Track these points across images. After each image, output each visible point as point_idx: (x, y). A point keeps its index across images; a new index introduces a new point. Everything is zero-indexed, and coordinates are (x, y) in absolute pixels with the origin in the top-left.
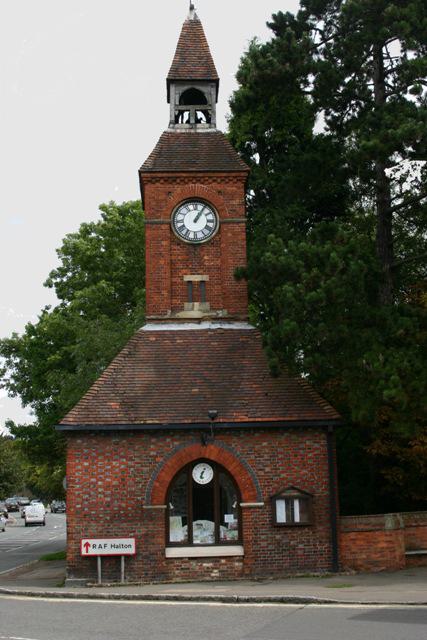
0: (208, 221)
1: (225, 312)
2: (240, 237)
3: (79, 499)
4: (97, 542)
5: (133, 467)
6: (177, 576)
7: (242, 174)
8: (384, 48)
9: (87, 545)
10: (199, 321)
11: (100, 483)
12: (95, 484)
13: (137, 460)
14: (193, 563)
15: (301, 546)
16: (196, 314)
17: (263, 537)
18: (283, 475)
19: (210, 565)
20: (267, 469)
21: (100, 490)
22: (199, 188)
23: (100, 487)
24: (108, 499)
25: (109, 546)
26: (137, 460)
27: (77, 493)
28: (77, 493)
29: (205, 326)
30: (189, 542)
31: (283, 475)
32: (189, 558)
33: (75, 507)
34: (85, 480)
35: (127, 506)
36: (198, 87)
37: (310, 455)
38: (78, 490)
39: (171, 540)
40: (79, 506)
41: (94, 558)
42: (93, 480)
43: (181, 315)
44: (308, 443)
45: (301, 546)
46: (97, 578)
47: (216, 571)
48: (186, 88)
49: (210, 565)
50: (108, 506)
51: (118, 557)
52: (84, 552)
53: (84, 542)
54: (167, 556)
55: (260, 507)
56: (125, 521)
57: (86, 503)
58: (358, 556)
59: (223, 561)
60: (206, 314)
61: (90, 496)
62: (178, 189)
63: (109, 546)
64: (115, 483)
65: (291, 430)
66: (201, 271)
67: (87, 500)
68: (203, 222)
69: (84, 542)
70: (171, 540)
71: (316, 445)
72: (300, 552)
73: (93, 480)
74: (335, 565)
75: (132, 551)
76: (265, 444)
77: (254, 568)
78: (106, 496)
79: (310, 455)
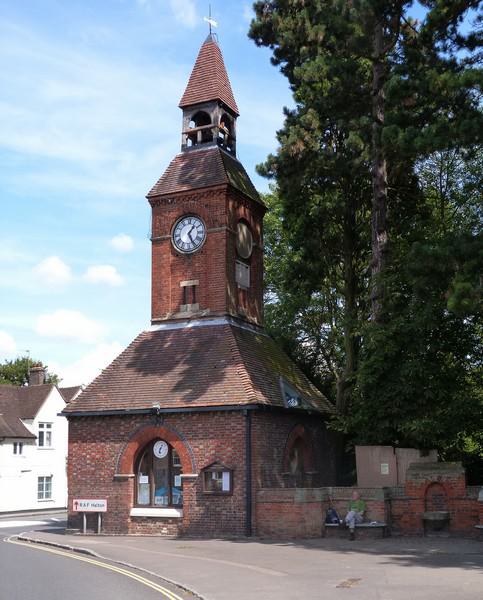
0: (198, 232)
1: (208, 310)
4: (83, 501)
8: (401, 19)
9: (76, 503)
10: (189, 320)
16: (187, 315)
20: (201, 447)
30: (150, 505)
36: (203, 110)
37: (234, 435)
41: (81, 513)
44: (233, 424)
45: (224, 512)
46: (83, 528)
48: (195, 112)
51: (97, 514)
52: (74, 509)
53: (74, 501)
55: (195, 478)
58: (271, 524)
64: (97, 456)
68: (185, 238)
69: (74, 501)
71: (239, 427)
74: (249, 529)
75: (104, 509)
76: (200, 425)
77: (186, 532)
79: (234, 435)
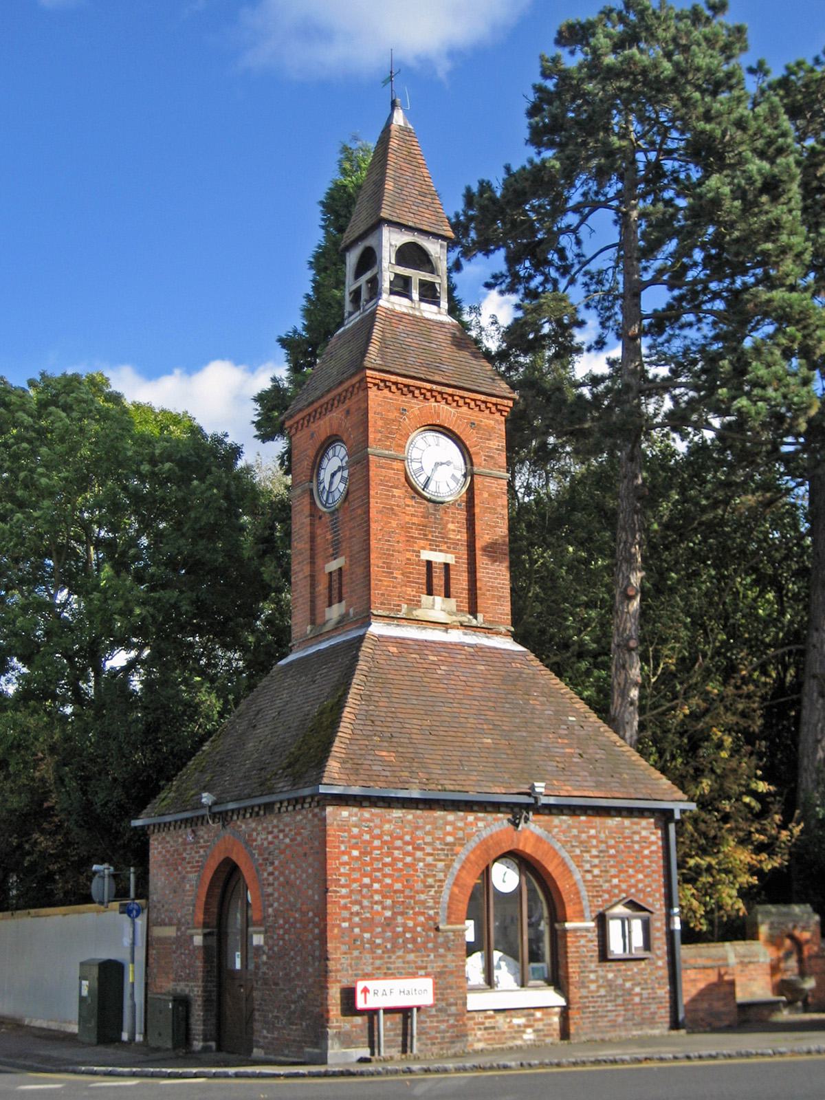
2: (500, 502)
3: (346, 914)
5: (424, 860)
6: (479, 1040)
7: (505, 402)
10: (446, 626)
11: (376, 886)
12: (369, 886)
13: (429, 849)
14: (500, 1018)
15: (637, 990)
17: (592, 976)
18: (615, 881)
19: (522, 1021)
20: (596, 871)
21: (377, 897)
22: (447, 413)
23: (376, 892)
24: (388, 914)
25: (396, 992)
26: (429, 849)
27: (343, 902)
28: (343, 902)
29: (455, 636)
31: (615, 881)
32: (496, 1011)
33: (339, 926)
34: (355, 881)
35: (416, 925)
38: (343, 897)
39: (366, 1018)
40: (345, 925)
42: (367, 880)
43: (419, 613)
45: (637, 990)
47: (529, 1030)
49: (522, 1021)
50: (388, 925)
54: (469, 1007)
56: (412, 951)
57: (357, 919)
59: (538, 1014)
60: (454, 618)
61: (362, 908)
62: (416, 406)
63: (396, 992)
65: (624, 813)
66: (444, 547)
67: (358, 914)
70: (366, 1018)
72: (637, 999)
73: (367, 880)
75: (427, 999)
78: (384, 908)
